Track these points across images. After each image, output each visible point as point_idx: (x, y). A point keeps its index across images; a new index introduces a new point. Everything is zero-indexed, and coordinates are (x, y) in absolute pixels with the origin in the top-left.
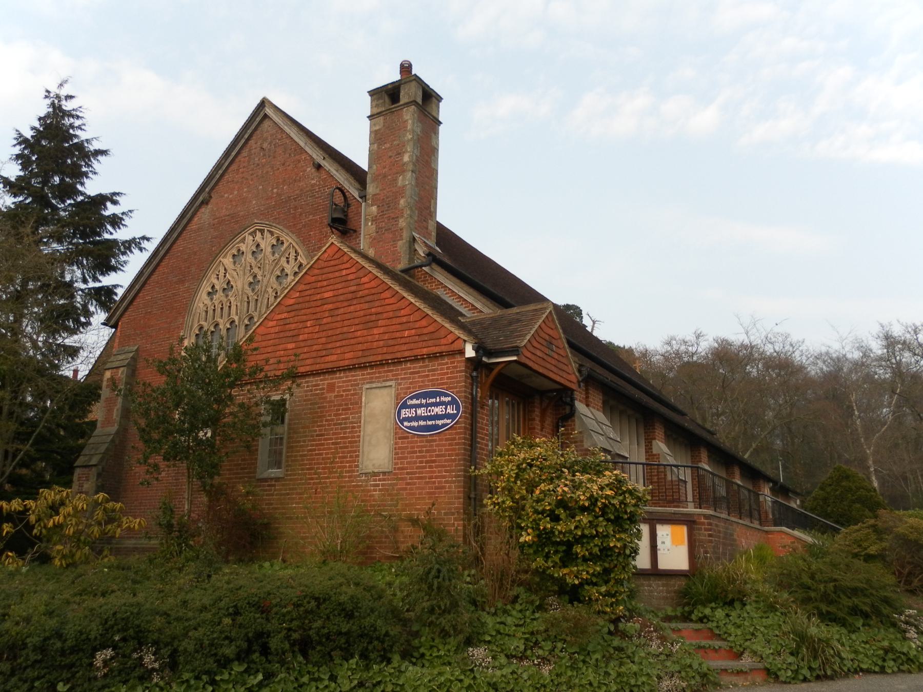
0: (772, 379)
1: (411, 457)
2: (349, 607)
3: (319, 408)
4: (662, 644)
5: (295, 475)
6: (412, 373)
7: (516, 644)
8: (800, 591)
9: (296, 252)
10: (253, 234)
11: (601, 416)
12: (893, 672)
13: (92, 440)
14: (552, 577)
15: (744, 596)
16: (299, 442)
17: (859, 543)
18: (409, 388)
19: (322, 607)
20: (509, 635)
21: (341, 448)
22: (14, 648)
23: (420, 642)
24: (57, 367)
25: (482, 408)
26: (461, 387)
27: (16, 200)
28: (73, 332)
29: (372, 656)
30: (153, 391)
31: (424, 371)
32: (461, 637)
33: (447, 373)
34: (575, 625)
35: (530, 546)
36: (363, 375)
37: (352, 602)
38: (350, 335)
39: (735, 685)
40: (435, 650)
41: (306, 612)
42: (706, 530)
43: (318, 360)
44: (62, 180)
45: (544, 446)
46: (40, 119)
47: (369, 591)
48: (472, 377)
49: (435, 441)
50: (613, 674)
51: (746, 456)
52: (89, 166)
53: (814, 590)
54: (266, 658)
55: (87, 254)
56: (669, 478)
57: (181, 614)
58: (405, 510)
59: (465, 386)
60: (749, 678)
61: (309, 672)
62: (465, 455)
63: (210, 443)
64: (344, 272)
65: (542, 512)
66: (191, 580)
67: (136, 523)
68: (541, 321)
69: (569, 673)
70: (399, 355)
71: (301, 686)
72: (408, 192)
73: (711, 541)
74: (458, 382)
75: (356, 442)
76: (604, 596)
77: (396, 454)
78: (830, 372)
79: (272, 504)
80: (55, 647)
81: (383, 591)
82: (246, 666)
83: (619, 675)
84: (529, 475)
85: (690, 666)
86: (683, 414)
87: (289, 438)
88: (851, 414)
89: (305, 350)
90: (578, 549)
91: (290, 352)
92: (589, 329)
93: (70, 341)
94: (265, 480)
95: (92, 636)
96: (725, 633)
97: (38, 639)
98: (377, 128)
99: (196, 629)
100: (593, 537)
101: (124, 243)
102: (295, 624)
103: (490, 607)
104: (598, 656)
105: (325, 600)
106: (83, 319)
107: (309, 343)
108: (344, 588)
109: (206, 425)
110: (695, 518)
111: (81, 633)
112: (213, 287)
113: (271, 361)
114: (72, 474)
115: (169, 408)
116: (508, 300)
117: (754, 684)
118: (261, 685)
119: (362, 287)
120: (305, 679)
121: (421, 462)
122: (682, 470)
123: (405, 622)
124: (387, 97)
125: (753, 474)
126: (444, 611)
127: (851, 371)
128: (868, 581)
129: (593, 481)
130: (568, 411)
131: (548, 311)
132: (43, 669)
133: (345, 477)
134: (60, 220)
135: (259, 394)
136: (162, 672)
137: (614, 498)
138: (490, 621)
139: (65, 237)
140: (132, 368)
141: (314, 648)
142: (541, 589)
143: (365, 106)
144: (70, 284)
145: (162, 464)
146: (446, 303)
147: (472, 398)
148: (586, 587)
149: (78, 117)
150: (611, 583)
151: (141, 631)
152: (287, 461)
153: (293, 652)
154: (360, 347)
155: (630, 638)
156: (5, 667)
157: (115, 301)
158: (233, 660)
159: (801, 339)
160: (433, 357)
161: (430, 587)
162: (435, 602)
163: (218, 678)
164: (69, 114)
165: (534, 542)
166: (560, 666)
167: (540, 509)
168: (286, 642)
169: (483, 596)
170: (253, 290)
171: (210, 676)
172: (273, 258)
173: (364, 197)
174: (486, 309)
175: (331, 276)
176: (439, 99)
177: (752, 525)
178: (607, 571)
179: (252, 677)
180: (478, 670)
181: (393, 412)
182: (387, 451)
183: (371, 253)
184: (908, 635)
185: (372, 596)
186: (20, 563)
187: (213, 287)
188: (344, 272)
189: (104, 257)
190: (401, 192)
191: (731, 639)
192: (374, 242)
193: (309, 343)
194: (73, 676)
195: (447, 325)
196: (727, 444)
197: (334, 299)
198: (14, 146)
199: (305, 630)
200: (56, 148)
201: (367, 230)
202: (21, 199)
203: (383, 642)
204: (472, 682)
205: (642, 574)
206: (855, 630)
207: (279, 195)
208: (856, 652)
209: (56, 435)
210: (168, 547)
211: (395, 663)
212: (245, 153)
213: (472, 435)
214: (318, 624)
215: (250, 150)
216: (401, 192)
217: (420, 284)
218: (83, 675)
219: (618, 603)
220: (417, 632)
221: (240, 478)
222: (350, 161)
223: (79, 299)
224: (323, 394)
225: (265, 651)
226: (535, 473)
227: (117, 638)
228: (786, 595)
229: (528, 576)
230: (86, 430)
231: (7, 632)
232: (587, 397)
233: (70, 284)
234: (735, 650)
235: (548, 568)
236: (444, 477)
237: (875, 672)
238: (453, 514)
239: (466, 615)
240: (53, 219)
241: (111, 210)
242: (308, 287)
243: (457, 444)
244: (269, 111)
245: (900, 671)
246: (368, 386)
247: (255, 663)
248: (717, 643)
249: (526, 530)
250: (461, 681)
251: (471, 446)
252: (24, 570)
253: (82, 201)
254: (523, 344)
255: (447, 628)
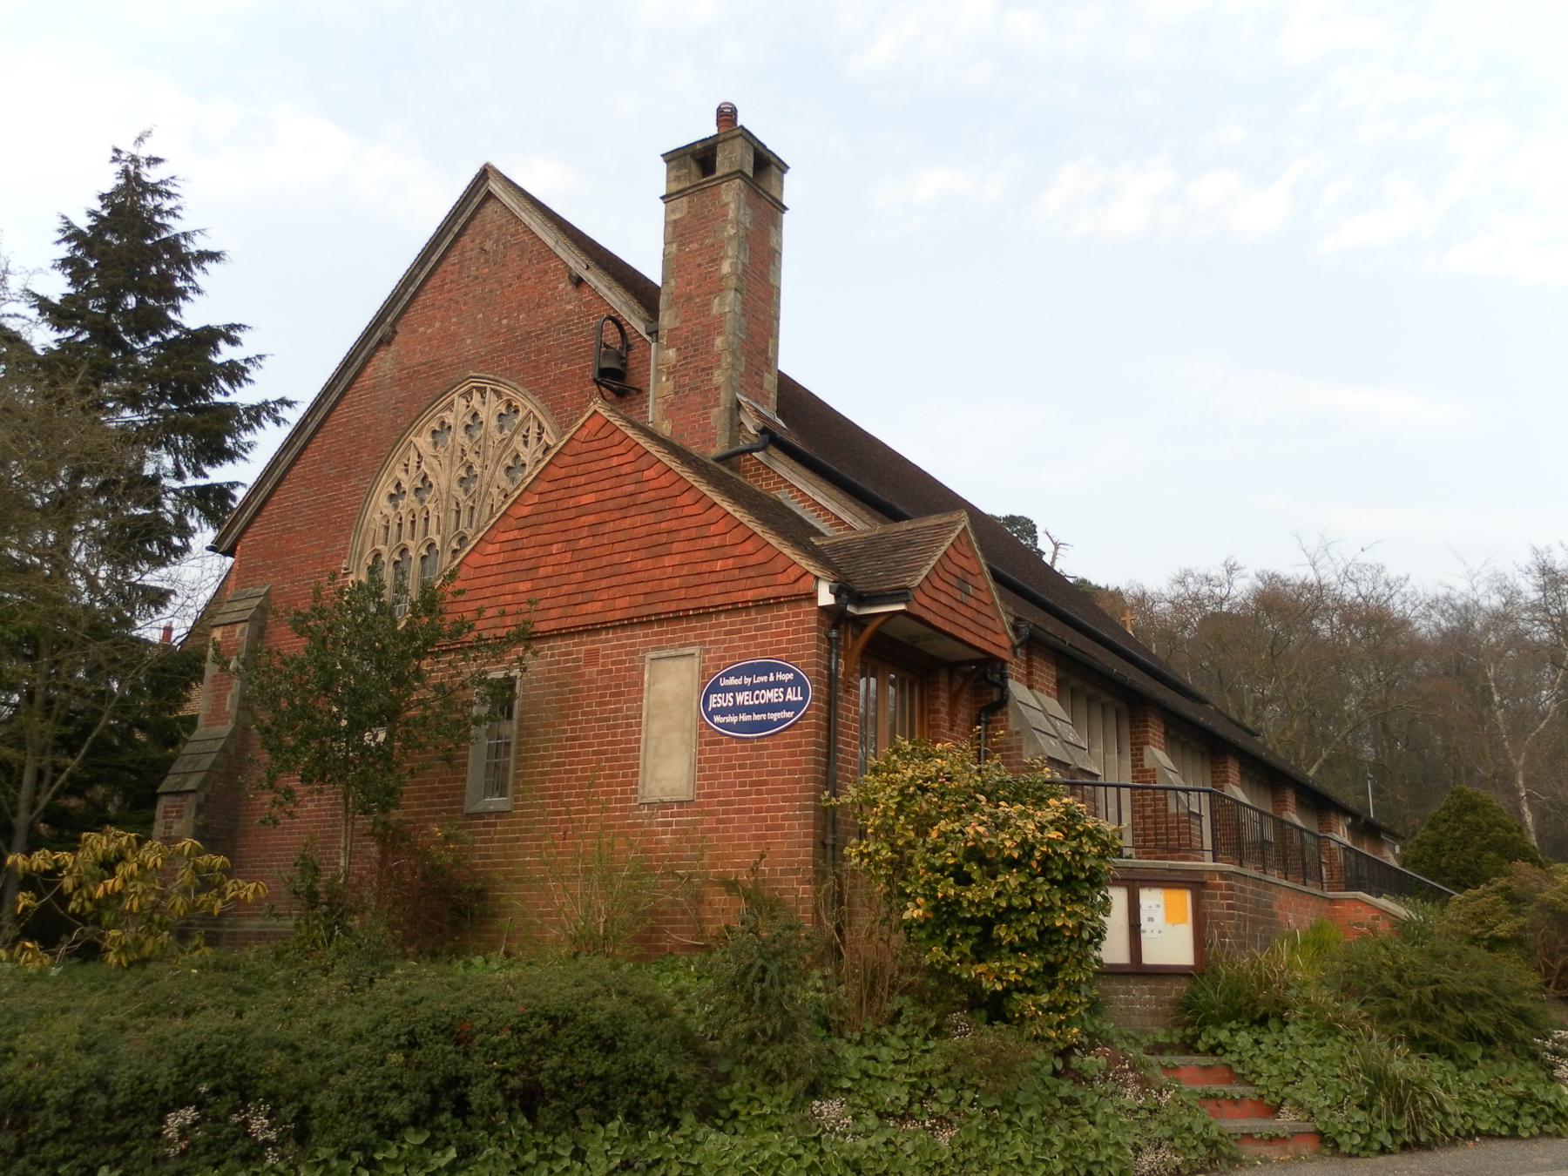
0: (1355, 641)
1: (727, 776)
2: (607, 1032)
3: (571, 692)
4: (1143, 1091)
5: (529, 806)
6: (727, 633)
7: (894, 1094)
8: (1378, 1000)
9: (540, 426)
10: (467, 395)
11: (1053, 705)
12: (1532, 1136)
13: (188, 748)
14: (957, 978)
15: (1286, 1009)
16: (537, 750)
17: (1479, 918)
18: (723, 658)
19: (561, 1033)
20: (883, 1079)
21: (607, 760)
22: (23, 1109)
23: (731, 1092)
24: (129, 624)
25: (847, 692)
26: (810, 656)
27: (61, 336)
28: (158, 562)
29: (646, 1116)
30: (284, 663)
31: (749, 630)
32: (799, 1083)
33: (787, 633)
34: (995, 1062)
35: (921, 927)
36: (646, 635)
37: (613, 1024)
38: (625, 568)
39: (1266, 1161)
40: (756, 1104)
41: (534, 1041)
42: (1224, 897)
43: (570, 611)
44: (140, 302)
45: (950, 757)
46: (102, 197)
47: (644, 1005)
48: (829, 639)
49: (766, 748)
50: (1059, 1145)
51: (1311, 773)
52: (187, 278)
53: (1401, 999)
54: (464, 1120)
55: (185, 429)
56: (1172, 809)
57: (318, 1047)
58: (713, 866)
59: (818, 656)
60: (1290, 1148)
61: (537, 1145)
62: (817, 771)
63: (383, 754)
64: (615, 462)
65: (942, 869)
66: (340, 988)
67: (248, 890)
68: (947, 544)
69: (984, 1143)
70: (706, 602)
71: (522, 1169)
72: (728, 327)
73: (1231, 917)
74: (805, 648)
75: (632, 750)
76: (1046, 1011)
77: (701, 770)
78: (1453, 629)
79: (489, 857)
80: (96, 1105)
81: (670, 1004)
82: (428, 1134)
83: (1069, 1144)
84: (921, 805)
85: (1189, 1129)
86: (1200, 700)
87: (519, 744)
88: (1488, 701)
89: (549, 593)
90: (1001, 931)
91: (524, 597)
92: (1047, 559)
93: (154, 578)
94: (479, 815)
95: (159, 1086)
96: (1252, 1072)
97: (64, 1091)
98: (677, 216)
99: (342, 1072)
100: (1027, 911)
101: (248, 410)
102: (514, 1061)
103: (852, 1031)
104: (1032, 1113)
105: (566, 1020)
106: (176, 541)
107: (554, 581)
108: (599, 1001)
109: (375, 719)
110: (1206, 878)
111: (141, 1081)
112: (398, 486)
113: (489, 613)
114: (154, 806)
115: (311, 692)
116: (902, 509)
117: (1297, 1158)
118: (452, 1167)
119: (646, 486)
120: (530, 1157)
121: (743, 784)
122: (1193, 796)
123: (705, 1059)
124: (695, 163)
125: (1319, 803)
126: (773, 1038)
127: (1486, 629)
128: (1491, 983)
129: (1029, 816)
130: (995, 696)
131: (960, 527)
132: (74, 1143)
133: (615, 810)
134: (138, 370)
135: (469, 669)
136: (282, 1146)
137: (1062, 844)
138: (850, 1054)
139: (145, 399)
140: (259, 624)
141: (547, 1104)
142: (939, 1000)
143: (658, 178)
144: (155, 480)
145: (301, 789)
146: (792, 513)
147: (830, 676)
148: (1016, 996)
149: (169, 195)
150: (1061, 986)
151: (244, 1077)
152: (516, 784)
153: (510, 1111)
154: (642, 588)
155: (1090, 1081)
156: (7, 1141)
157: (232, 509)
158: (405, 1126)
159: (1403, 575)
160: (764, 605)
161: (749, 998)
162: (755, 1023)
163: (379, 1156)
164: (155, 190)
165: (927, 920)
166: (969, 1131)
167: (938, 863)
168: (498, 1094)
169: (840, 1013)
170: (466, 491)
171: (365, 1152)
172: (500, 437)
173: (654, 333)
174: (855, 523)
175: (593, 467)
176: (783, 167)
177: (1305, 889)
178: (1051, 969)
179: (438, 1154)
180: (828, 1138)
181: (695, 699)
182: (686, 766)
183: (666, 429)
184: (1557, 1073)
185: (647, 1013)
186: (47, 960)
187: (398, 486)
188: (615, 462)
189: (213, 435)
190: (716, 326)
191: (1261, 1082)
192: (670, 410)
193: (554, 581)
194: (127, 1155)
195: (788, 551)
196: (1281, 754)
197: (598, 507)
198: (58, 242)
199: (531, 1073)
200: (129, 250)
201: (659, 388)
202: (70, 333)
203: (665, 1092)
204: (816, 1160)
205: (1115, 972)
206: (1471, 1066)
207: (510, 329)
208: (1469, 1103)
209: (118, 739)
210: (310, 931)
211: (686, 1129)
212: (453, 258)
213: (828, 738)
214: (555, 1061)
215: (462, 253)
216: (716, 326)
217: (749, 482)
218: (144, 1153)
219: (1069, 1022)
220: (727, 1075)
221: (437, 812)
222: (635, 272)
223: (169, 505)
224: (578, 668)
225: (462, 1108)
226: (929, 802)
227: (203, 1089)
228: (1354, 1008)
229: (917, 978)
230: (171, 734)
231: (11, 1080)
232: (1030, 673)
233: (155, 480)
234: (1267, 1101)
235: (952, 963)
236: (781, 809)
237: (1501, 1137)
238: (797, 871)
239: (810, 1045)
240: (125, 369)
241: (225, 353)
242: (553, 486)
243: (802, 753)
244: (494, 186)
245: (1543, 1134)
246: (653, 655)
247: (444, 1130)
248: (1238, 1090)
249: (914, 900)
250: (797, 1157)
251: (828, 756)
252: (54, 972)
253: (176, 338)
254: (916, 583)
255: (776, 1067)
